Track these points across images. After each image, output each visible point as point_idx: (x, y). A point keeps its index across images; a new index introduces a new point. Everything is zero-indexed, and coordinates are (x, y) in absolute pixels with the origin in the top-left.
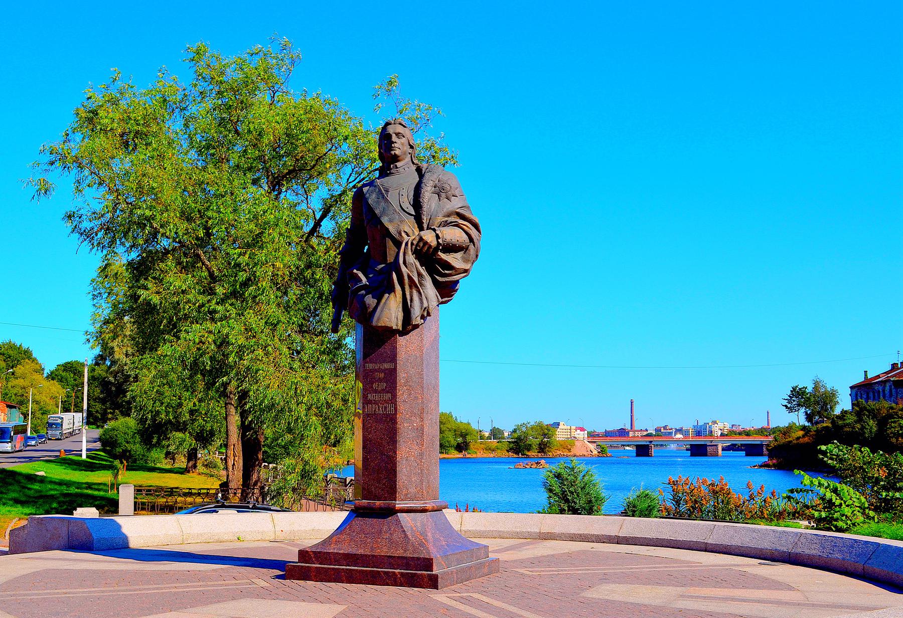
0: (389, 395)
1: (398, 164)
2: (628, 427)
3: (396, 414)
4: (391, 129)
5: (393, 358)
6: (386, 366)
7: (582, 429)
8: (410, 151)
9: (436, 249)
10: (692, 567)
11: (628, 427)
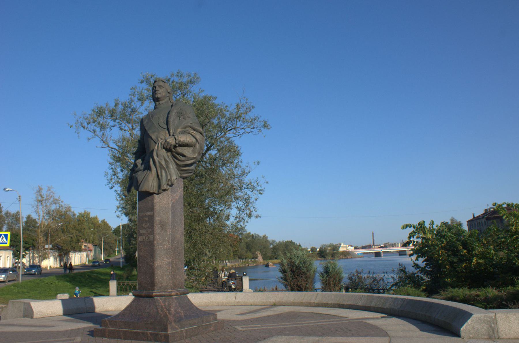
0: (150, 230)
1: (161, 102)
2: (372, 244)
3: (154, 241)
4: (156, 85)
5: (152, 209)
6: (149, 213)
7: (352, 246)
8: (168, 95)
9: (175, 147)
10: (343, 320)
11: (372, 244)
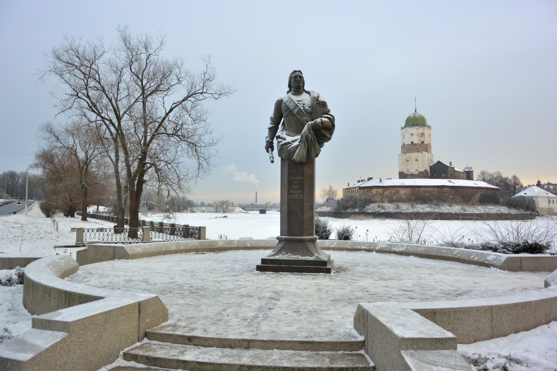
6: (299, 178)
